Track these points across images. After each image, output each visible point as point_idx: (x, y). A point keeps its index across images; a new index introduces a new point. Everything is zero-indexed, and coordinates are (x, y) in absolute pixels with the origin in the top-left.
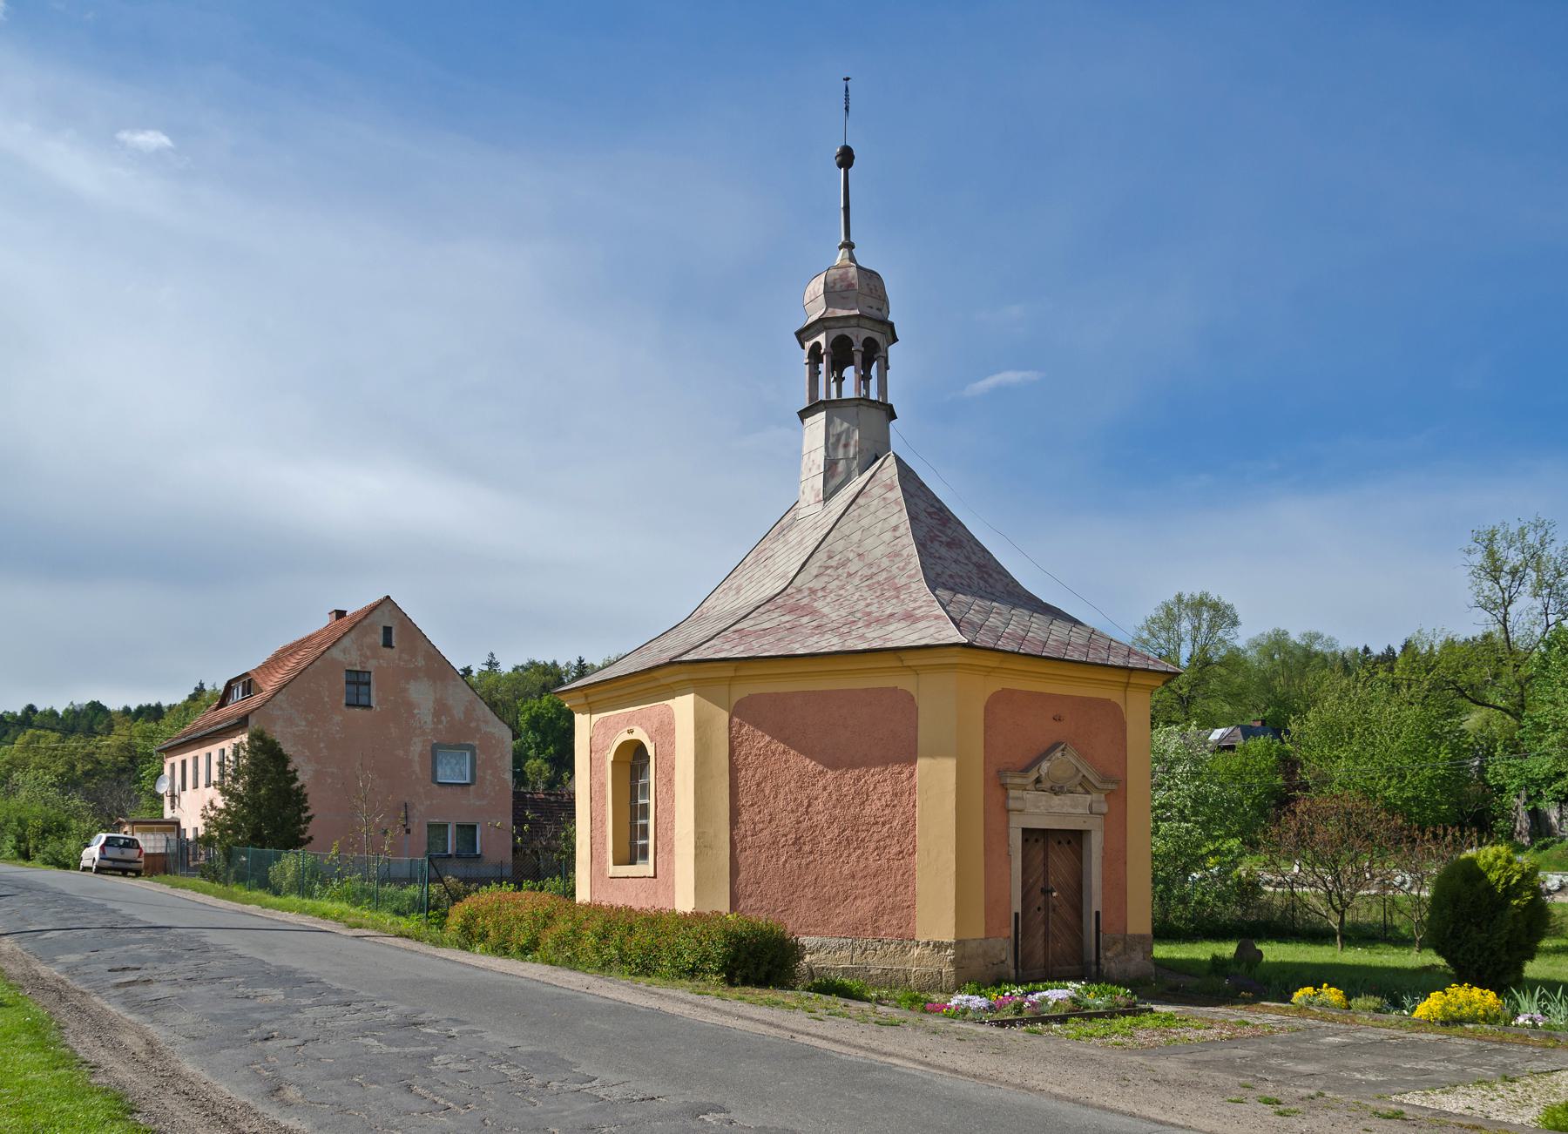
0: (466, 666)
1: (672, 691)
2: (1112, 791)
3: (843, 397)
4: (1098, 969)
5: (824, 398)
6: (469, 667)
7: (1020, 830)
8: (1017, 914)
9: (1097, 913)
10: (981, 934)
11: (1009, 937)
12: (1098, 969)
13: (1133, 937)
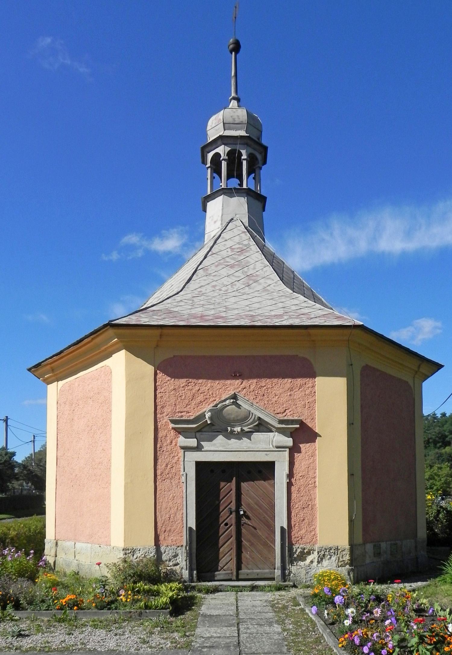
5: (246, 187)
7: (195, 462)
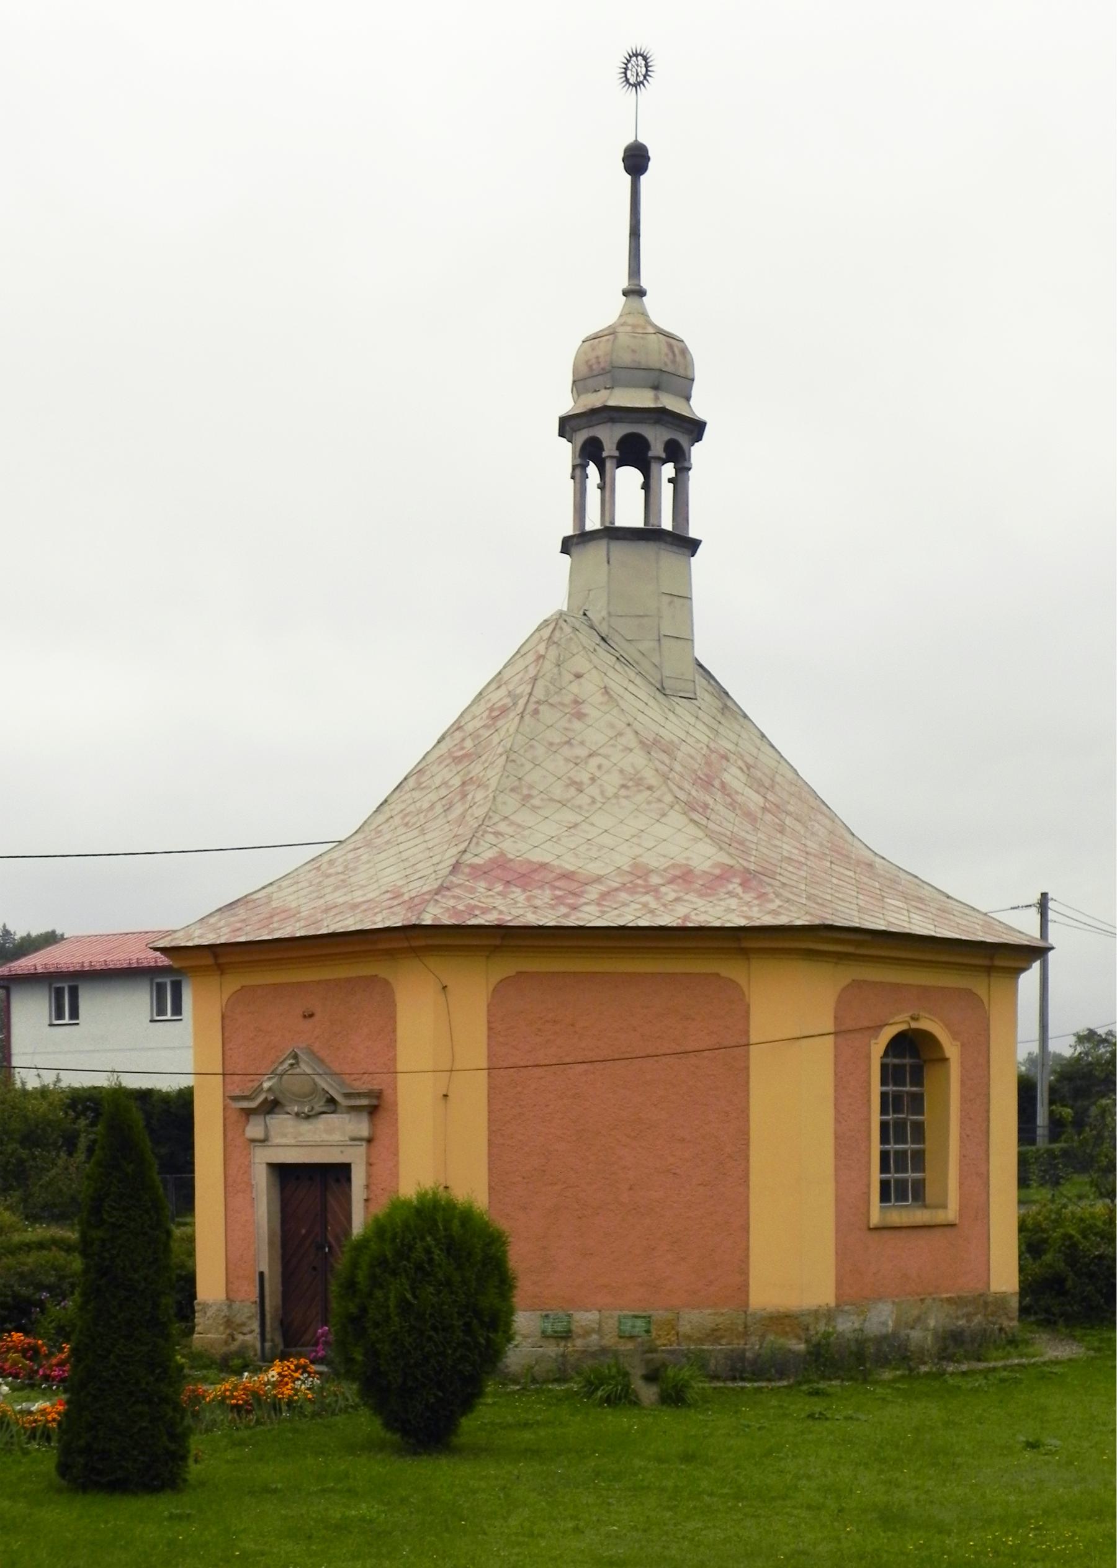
7: (264, 1166)
10: (222, 1296)
11: (256, 1302)
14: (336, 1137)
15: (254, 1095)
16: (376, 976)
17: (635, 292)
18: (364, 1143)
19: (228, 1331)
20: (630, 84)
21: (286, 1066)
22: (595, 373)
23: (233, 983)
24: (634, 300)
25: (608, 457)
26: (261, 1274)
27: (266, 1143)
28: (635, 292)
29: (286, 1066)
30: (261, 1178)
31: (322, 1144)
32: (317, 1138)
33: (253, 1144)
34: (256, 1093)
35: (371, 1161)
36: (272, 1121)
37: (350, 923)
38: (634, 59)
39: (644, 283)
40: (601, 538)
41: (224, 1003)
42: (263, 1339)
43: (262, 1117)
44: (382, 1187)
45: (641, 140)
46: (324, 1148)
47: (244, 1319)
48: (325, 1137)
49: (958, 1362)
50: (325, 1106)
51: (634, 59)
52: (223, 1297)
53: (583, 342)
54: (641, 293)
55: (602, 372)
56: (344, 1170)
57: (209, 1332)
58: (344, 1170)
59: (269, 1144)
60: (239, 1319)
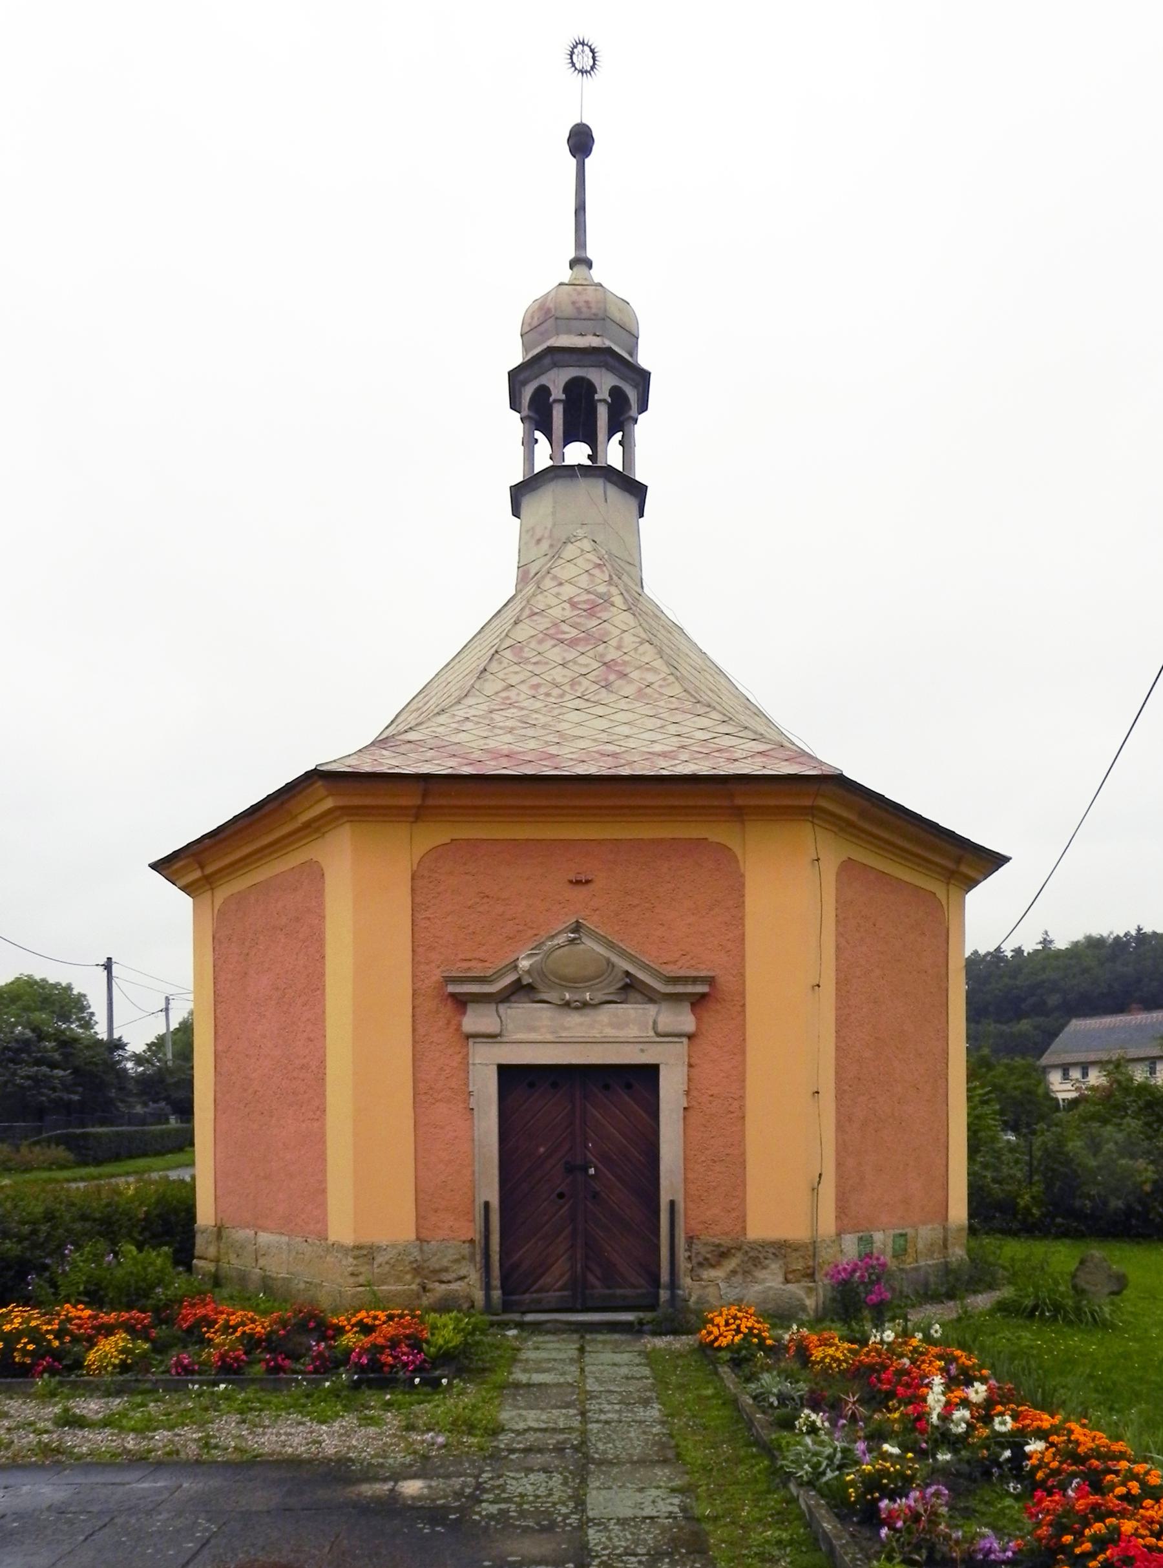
0: (1017, 946)
1: (315, 828)
2: (703, 996)
3: (567, 463)
4: (673, 1296)
6: (1020, 948)
7: (495, 1068)
8: (487, 1205)
9: (672, 1204)
10: (408, 1234)
11: (472, 1241)
12: (673, 1296)
13: (764, 1245)
14: (632, 1032)
15: (494, 977)
16: (706, 839)
17: (581, 261)
18: (685, 1040)
19: (418, 1280)
20: (576, 69)
21: (561, 939)
22: (583, 316)
23: (433, 835)
24: (581, 269)
25: (600, 401)
26: (487, 1205)
27: (499, 1039)
28: (581, 261)
29: (561, 939)
30: (487, 1087)
31: (604, 1040)
32: (595, 1033)
33: (471, 1040)
34: (499, 974)
35: (693, 1061)
36: (509, 1011)
37: (703, 768)
38: (580, 46)
39: (590, 254)
40: (599, 476)
41: (416, 861)
42: (488, 1287)
43: (493, 1006)
44: (710, 1093)
45: (584, 122)
46: (606, 1045)
47: (445, 1263)
48: (610, 1032)
49: (670, 1352)
50: (616, 993)
51: (580, 46)
52: (413, 1236)
53: (561, 284)
54: (589, 264)
55: (593, 317)
56: (650, 1073)
57: (384, 1283)
58: (650, 1073)
59: (504, 1039)
60: (434, 1263)
